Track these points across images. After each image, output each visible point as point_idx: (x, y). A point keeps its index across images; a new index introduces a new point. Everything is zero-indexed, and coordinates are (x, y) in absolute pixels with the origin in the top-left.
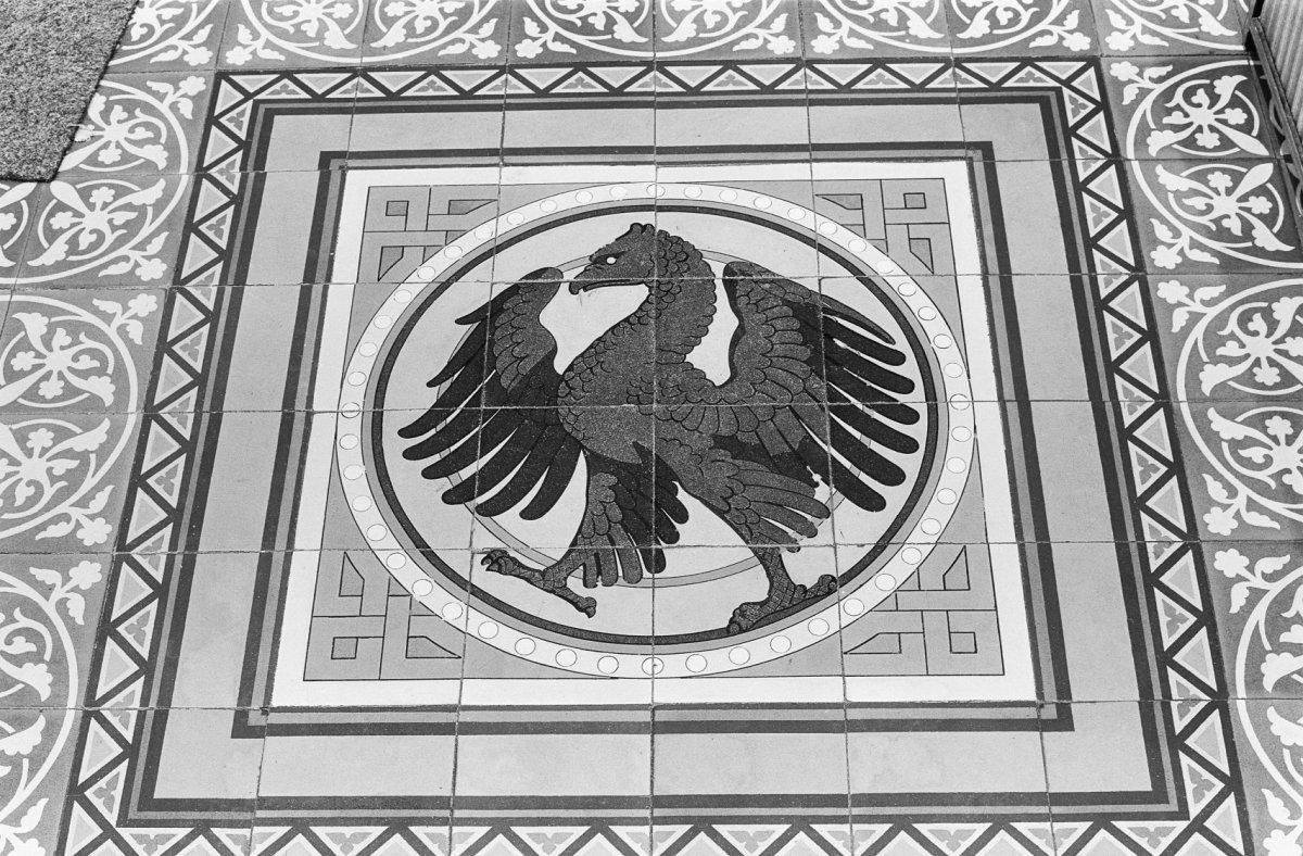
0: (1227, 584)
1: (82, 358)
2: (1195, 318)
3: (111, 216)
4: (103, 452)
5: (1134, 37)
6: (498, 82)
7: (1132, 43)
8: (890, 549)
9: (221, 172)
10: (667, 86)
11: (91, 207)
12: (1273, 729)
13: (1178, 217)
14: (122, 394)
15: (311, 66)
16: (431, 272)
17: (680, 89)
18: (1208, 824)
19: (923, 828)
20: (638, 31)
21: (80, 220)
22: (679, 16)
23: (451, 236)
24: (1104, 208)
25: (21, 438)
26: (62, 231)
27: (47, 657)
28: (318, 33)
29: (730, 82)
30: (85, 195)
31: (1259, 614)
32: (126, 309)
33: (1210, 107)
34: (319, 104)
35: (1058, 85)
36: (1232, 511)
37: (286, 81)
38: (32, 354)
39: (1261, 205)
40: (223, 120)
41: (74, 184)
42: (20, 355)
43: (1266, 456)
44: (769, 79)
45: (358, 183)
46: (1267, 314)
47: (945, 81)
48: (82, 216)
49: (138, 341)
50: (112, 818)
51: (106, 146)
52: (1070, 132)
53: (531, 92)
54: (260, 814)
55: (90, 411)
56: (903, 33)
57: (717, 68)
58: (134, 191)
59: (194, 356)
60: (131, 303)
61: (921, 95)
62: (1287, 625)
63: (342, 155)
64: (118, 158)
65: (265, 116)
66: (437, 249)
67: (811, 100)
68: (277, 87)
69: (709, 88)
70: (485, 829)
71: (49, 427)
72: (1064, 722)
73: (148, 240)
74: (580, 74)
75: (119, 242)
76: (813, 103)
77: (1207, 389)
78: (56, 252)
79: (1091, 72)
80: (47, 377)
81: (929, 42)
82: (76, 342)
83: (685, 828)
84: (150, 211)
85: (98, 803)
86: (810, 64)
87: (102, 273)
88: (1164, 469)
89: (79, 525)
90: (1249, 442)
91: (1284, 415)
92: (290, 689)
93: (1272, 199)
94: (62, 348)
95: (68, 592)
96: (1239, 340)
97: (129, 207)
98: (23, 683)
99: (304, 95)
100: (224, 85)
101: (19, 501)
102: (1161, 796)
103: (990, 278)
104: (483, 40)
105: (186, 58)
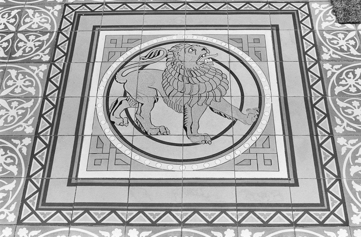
0: (326, 71)
2: (333, 74)
3: (34, 43)
4: (32, 108)
8: (248, 136)
9: (62, 47)
10: (189, 8)
11: (29, 41)
12: (353, 187)
13: (342, 115)
14: (20, 172)
16: (122, 59)
18: (336, 212)
19: (257, 213)
21: (26, 44)
23: (128, 49)
24: (309, 43)
25: (10, 104)
27: (16, 164)
30: (27, 37)
31: (334, 77)
32: (38, 69)
33: (353, 79)
34: (93, 13)
35: (297, 9)
36: (342, 127)
38: (13, 81)
39: (352, 42)
40: (67, 17)
41: (6, 100)
42: (9, 81)
43: (352, 112)
46: (353, 73)
47: (266, 8)
48: (26, 43)
49: (42, 78)
50: (34, 208)
51: (34, 23)
52: (300, 22)
54: (75, 207)
55: (28, 98)
58: (40, 36)
62: (357, 158)
63: (99, 26)
64: (37, 27)
65: (78, 16)
68: (81, 8)
71: (17, 101)
72: (296, 184)
73: (45, 50)
75: (37, 51)
77: (336, 93)
78: (19, 53)
79: (306, 6)
80: (17, 87)
82: (25, 78)
84: (45, 42)
85: (30, 204)
88: (324, 115)
89: (42, 57)
90: (333, 39)
91: (357, 100)
93: (355, 40)
94: (21, 79)
95: (39, 71)
96: (331, 17)
97: (39, 41)
98: (10, 171)
99: (89, 10)
100: (67, 7)
101: (9, 121)
102: (323, 204)
103: (286, 137)
105: (42, 59)
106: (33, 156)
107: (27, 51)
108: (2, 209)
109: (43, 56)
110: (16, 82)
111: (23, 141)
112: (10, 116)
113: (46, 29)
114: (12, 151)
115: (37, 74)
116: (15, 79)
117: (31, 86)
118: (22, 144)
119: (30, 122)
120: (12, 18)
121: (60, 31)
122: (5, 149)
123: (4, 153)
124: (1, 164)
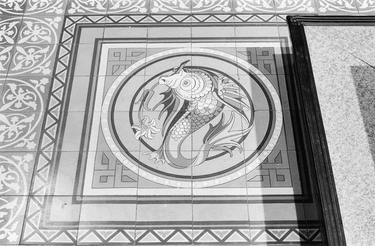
1: (27, 96)
3: (34, 56)
4: (33, 123)
5: (327, 9)
6: (189, 19)
7: (243, 10)
9: (63, 60)
15: (92, 14)
16: (127, 72)
17: (91, 22)
20: (104, 6)
21: (26, 57)
22: (33, 4)
23: (133, 62)
25: (9, 119)
26: (20, 61)
28: (12, 6)
29: (212, 19)
30: (26, 50)
34: (94, 25)
37: (170, 17)
38: (12, 95)
41: (23, 47)
42: (26, 31)
44: (202, 19)
45: (106, 48)
47: (274, 20)
48: (25, 56)
51: (33, 36)
53: (134, 22)
56: (177, 7)
57: (208, 16)
58: (40, 49)
59: (60, 96)
60: (41, 81)
61: (117, 25)
65: (79, 28)
66: (129, 66)
67: (191, 25)
69: (270, 21)
70: (174, 230)
71: (17, 116)
74: (85, 18)
75: (20, 136)
76: (236, 26)
78: (19, 67)
80: (17, 102)
81: (185, 10)
83: (174, 230)
86: (235, 15)
87: (32, 73)
89: (42, 70)
92: (88, 191)
94: (21, 93)
97: (39, 54)
100: (67, 19)
104: (59, 9)
105: (56, 12)
106: (51, 93)
107: (27, 65)
108: (3, 229)
109: (44, 69)
110: (32, 32)
111: (41, 81)
112: (10, 132)
113: (46, 41)
114: (13, 167)
115: (38, 88)
116: (31, 30)
117: (32, 100)
118: (24, 161)
119: (14, 227)
120: (11, 30)
121: (61, 44)
122: (6, 166)
123: (4, 170)
124: (2, 181)
